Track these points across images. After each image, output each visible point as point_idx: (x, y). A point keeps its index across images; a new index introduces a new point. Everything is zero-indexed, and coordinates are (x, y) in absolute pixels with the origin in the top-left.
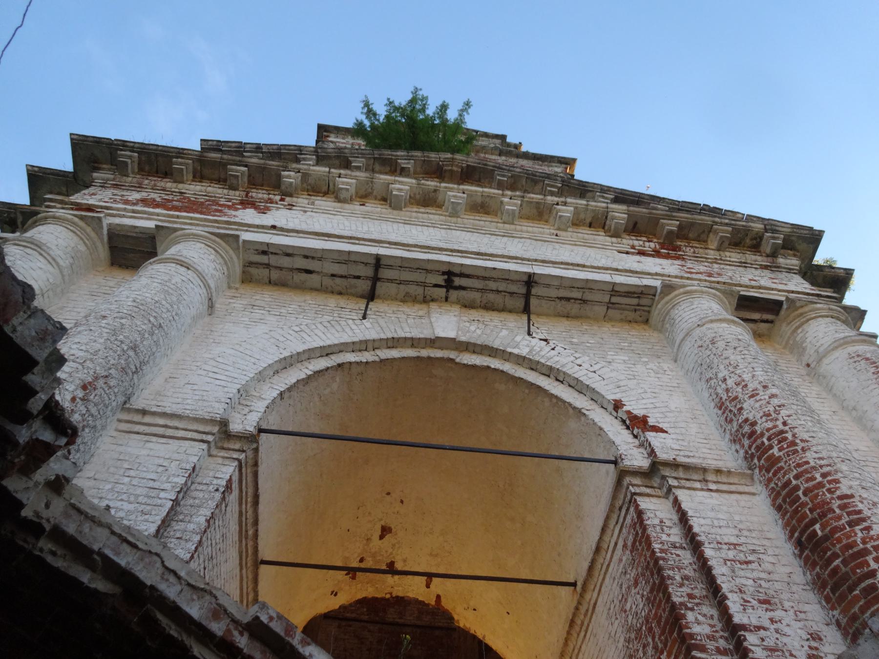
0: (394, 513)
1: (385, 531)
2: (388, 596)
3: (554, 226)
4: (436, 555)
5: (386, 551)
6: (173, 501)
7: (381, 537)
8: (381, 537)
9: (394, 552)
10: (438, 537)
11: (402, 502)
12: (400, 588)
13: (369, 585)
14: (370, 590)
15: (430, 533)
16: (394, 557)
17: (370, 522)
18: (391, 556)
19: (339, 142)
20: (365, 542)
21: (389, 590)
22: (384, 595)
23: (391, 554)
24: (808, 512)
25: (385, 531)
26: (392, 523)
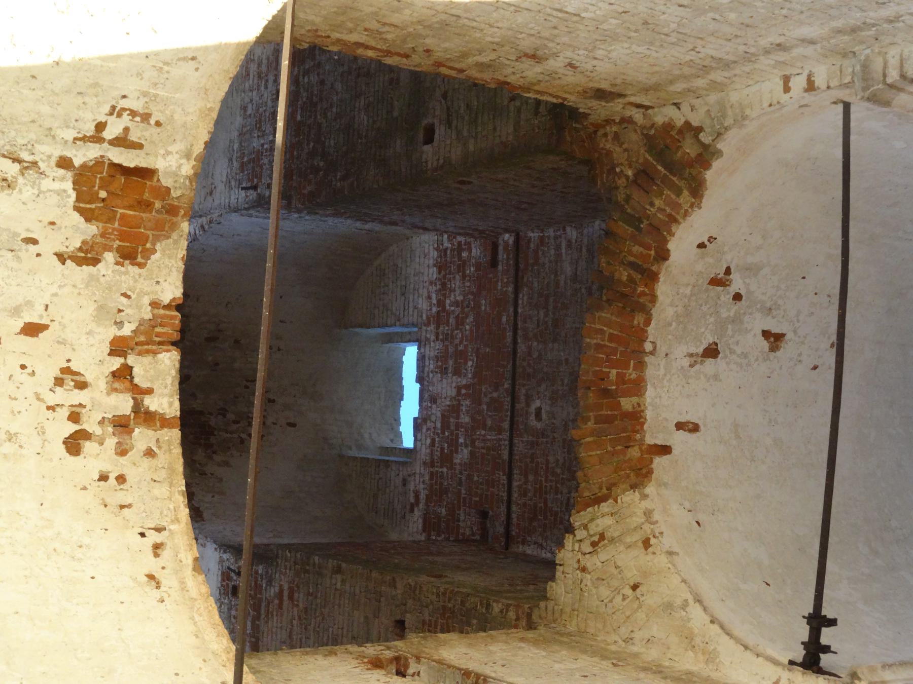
0: (800, 355)
1: (774, 339)
2: (648, 347)
3: (457, 372)
4: (738, 437)
5: (737, 343)
6: (179, 308)
7: (766, 334)
8: (766, 334)
9: (734, 357)
10: (768, 434)
11: (815, 368)
12: (662, 371)
13: (680, 309)
14: (670, 312)
15: (770, 421)
16: (726, 357)
17: (799, 313)
18: (728, 352)
19: (523, 302)
20: (768, 305)
21: (662, 349)
22: (651, 338)
23: (732, 352)
24: (118, 215)
25: (774, 339)
26: (787, 350)
